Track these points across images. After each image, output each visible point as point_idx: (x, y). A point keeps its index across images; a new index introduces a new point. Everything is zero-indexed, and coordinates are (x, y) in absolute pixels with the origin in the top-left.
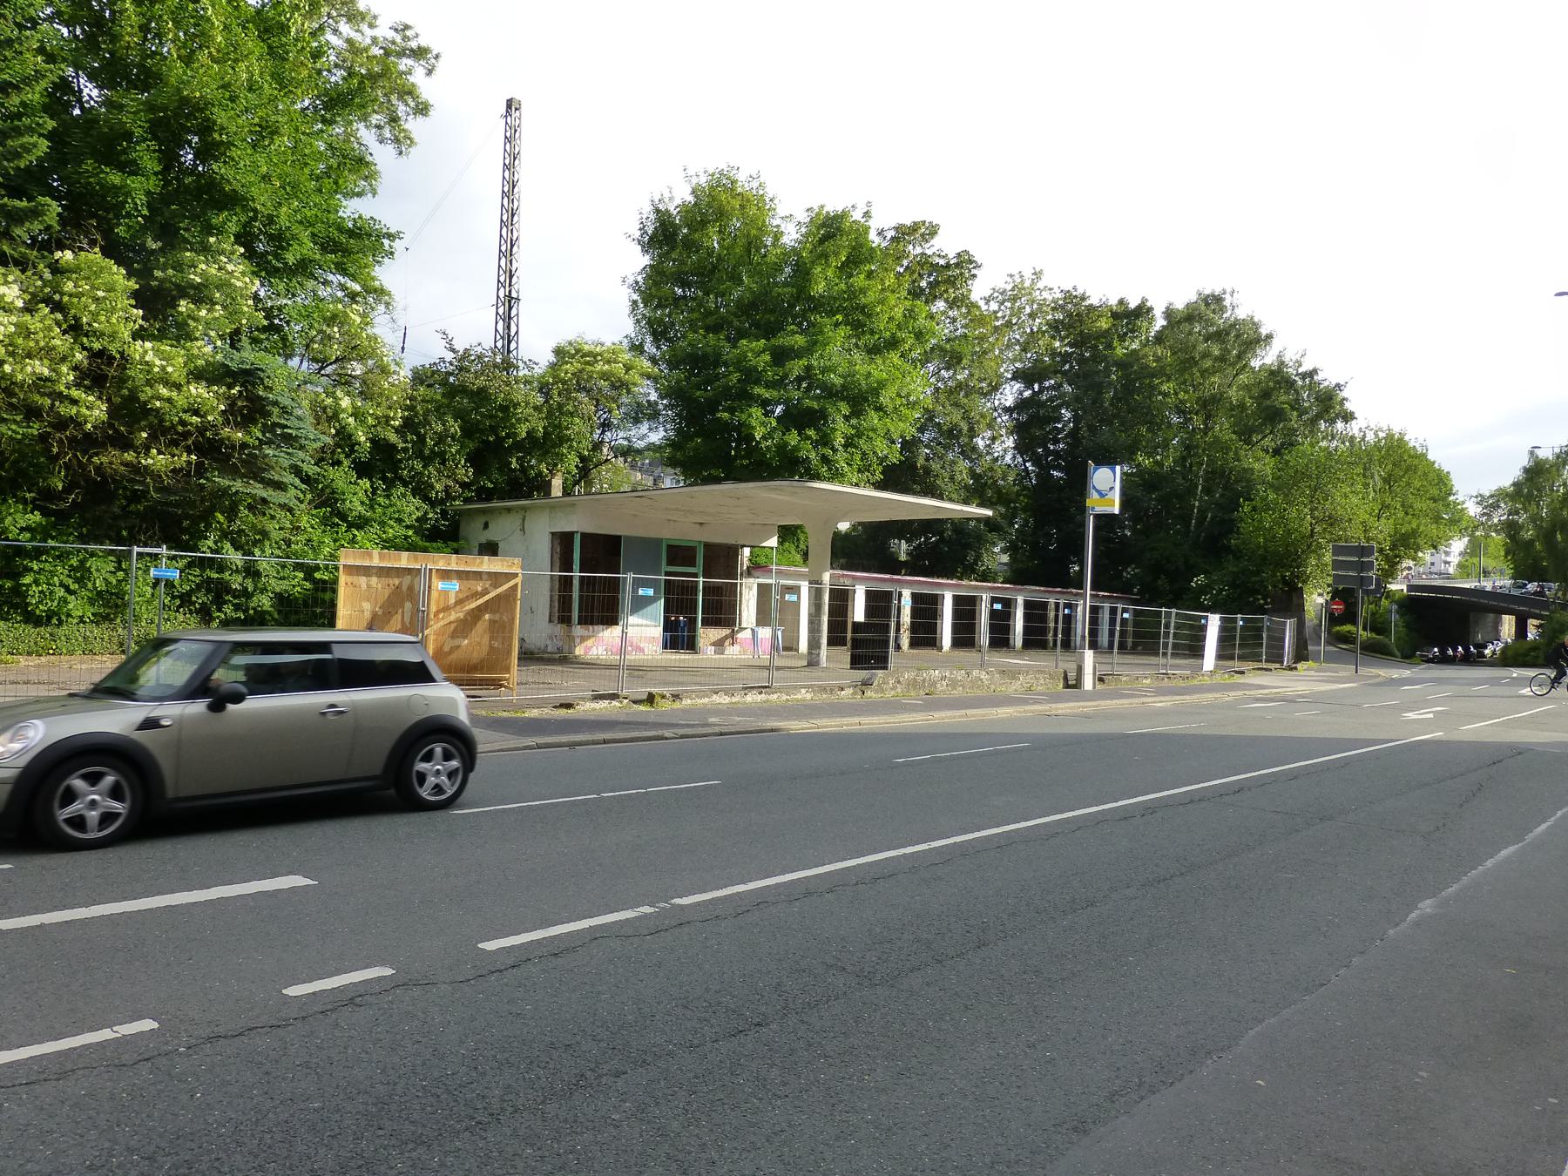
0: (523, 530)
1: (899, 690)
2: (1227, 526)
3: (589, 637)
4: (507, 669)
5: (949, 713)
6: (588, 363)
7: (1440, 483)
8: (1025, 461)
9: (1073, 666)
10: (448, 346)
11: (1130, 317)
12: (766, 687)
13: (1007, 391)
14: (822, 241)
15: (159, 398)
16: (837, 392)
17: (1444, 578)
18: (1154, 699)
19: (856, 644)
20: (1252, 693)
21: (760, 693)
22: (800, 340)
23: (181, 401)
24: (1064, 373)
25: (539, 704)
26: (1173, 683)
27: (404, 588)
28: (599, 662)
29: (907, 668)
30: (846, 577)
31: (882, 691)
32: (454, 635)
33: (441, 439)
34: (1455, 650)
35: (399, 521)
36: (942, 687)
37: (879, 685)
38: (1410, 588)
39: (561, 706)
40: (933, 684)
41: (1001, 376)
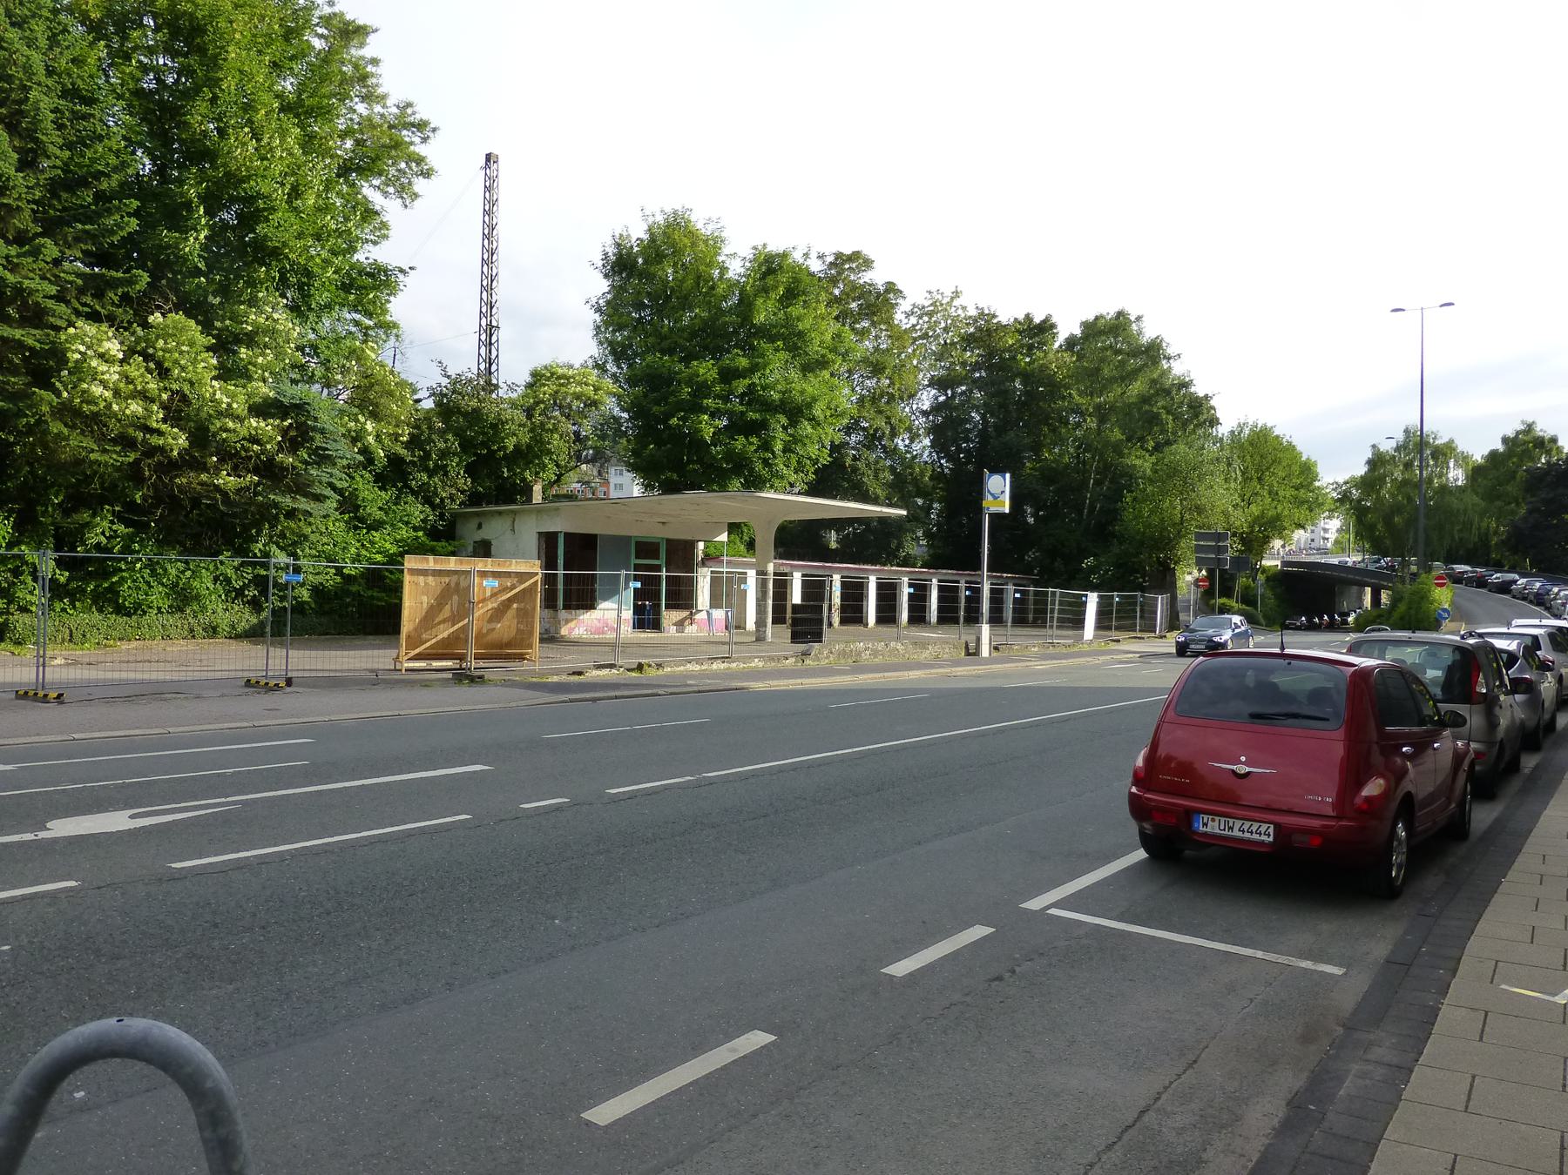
0: (513, 530)
1: (832, 659)
2: (1112, 515)
3: (572, 620)
4: (530, 646)
5: (871, 676)
6: (562, 385)
7: (1307, 471)
8: (939, 458)
9: (974, 638)
10: (443, 373)
11: (1039, 331)
12: (727, 658)
13: (924, 397)
14: (764, 276)
15: (227, 430)
16: (777, 406)
17: (1321, 554)
18: (1036, 663)
19: (795, 622)
20: (1118, 657)
21: (723, 662)
22: (743, 362)
23: (244, 432)
24: (975, 381)
25: (557, 672)
26: (1057, 650)
27: (453, 585)
28: (580, 641)
29: (838, 642)
30: (786, 564)
31: (818, 660)
32: (490, 620)
33: (444, 454)
34: (1321, 618)
35: (407, 523)
36: (866, 656)
37: (816, 655)
38: (1285, 564)
39: (574, 673)
40: (859, 654)
41: (919, 383)
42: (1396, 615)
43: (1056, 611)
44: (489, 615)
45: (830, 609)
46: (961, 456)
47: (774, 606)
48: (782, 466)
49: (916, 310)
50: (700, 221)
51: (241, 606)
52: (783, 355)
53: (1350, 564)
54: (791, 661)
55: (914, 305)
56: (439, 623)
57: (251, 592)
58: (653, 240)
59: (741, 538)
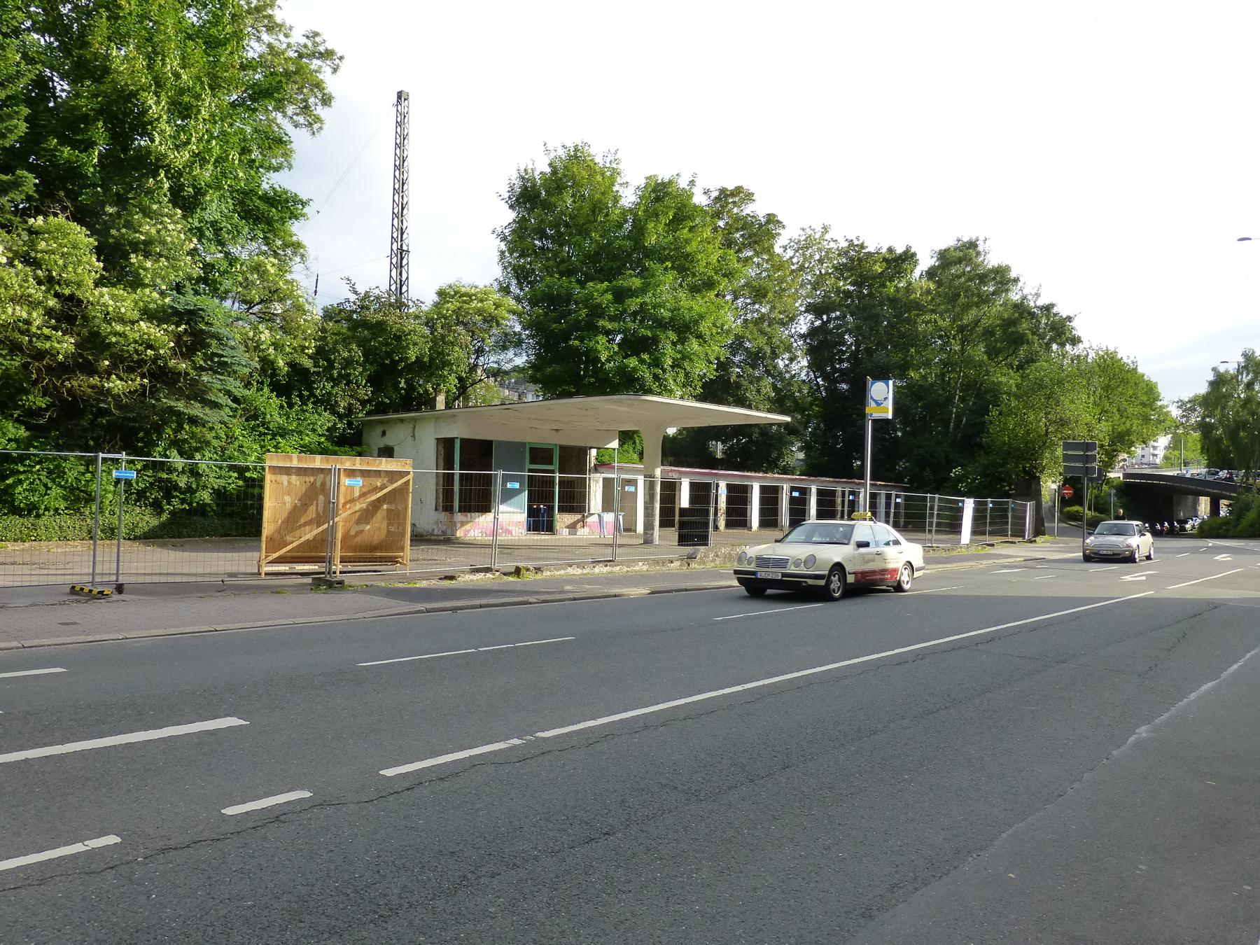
0: (414, 436)
1: (718, 562)
3: (467, 523)
4: (402, 549)
6: (465, 302)
7: (1151, 391)
8: (816, 377)
11: (900, 261)
12: (610, 561)
17: (1151, 468)
19: (682, 525)
22: (636, 282)
25: (427, 577)
26: (937, 554)
27: (318, 484)
28: (475, 542)
29: (724, 545)
30: (673, 472)
31: (704, 563)
32: (358, 522)
33: (348, 363)
34: (1162, 525)
37: (701, 558)
38: (1126, 476)
39: (446, 578)
42: (1244, 523)
44: (357, 517)
50: (599, 154)
51: (143, 508)
52: (671, 276)
53: (1188, 476)
54: (677, 564)
56: (305, 524)
57: (154, 495)
58: (554, 172)
59: (634, 448)
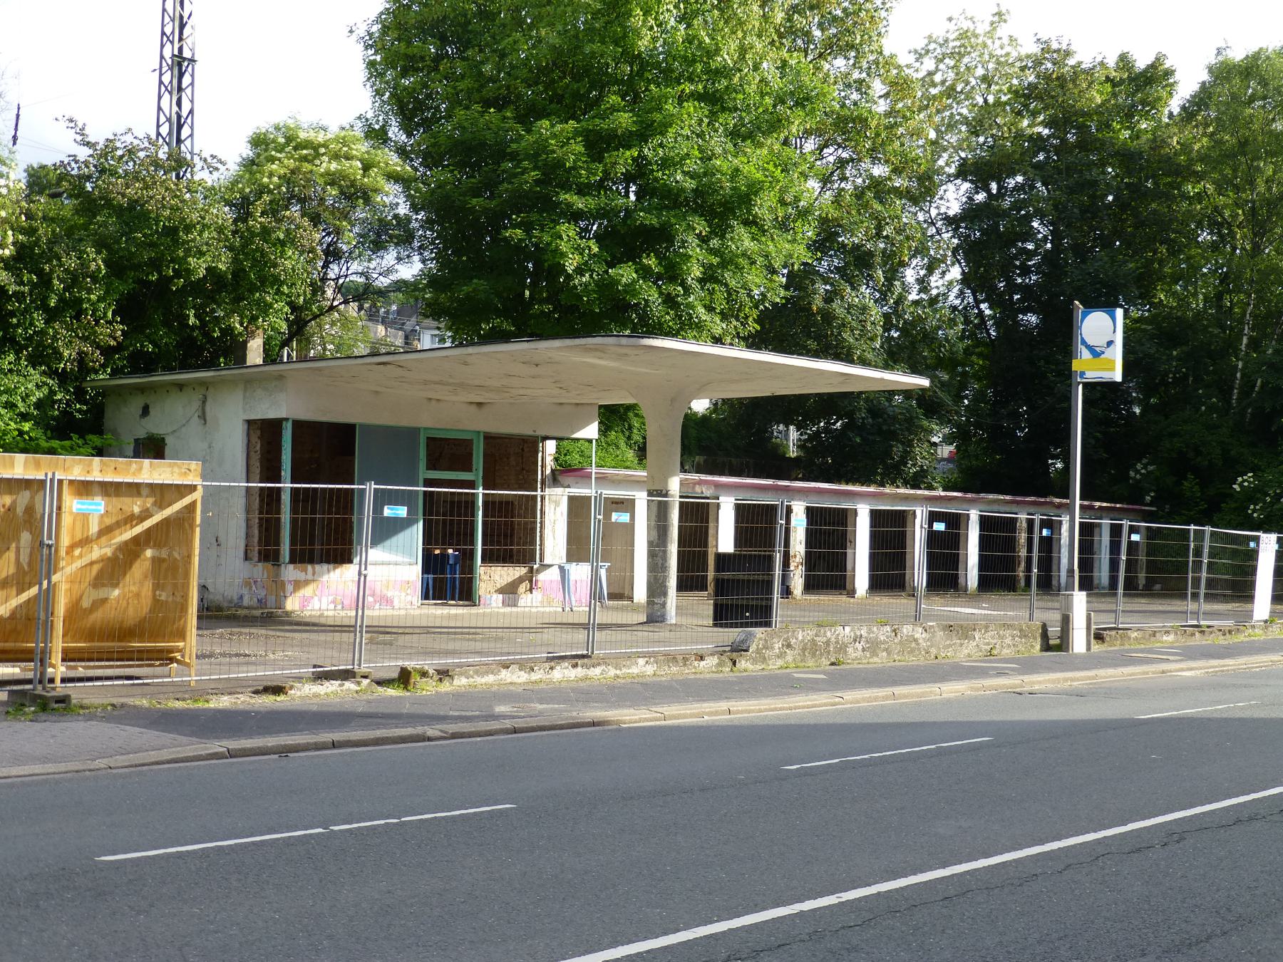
0: (203, 417)
1: (789, 658)
3: (307, 582)
4: (181, 635)
6: (305, 159)
8: (977, 302)
9: (1056, 616)
10: (79, 138)
12: (583, 657)
19: (722, 587)
21: (575, 666)
22: (625, 120)
25: (231, 688)
26: (1208, 640)
27: (20, 510)
28: (323, 621)
29: (802, 625)
30: (704, 484)
31: (764, 660)
32: (98, 582)
33: (74, 280)
36: (855, 652)
37: (758, 651)
40: (842, 648)
43: (1205, 567)
45: (786, 564)
46: (1016, 297)
47: (681, 555)
48: (701, 310)
49: (932, 46)
54: (711, 662)
55: (930, 37)
59: (629, 438)
